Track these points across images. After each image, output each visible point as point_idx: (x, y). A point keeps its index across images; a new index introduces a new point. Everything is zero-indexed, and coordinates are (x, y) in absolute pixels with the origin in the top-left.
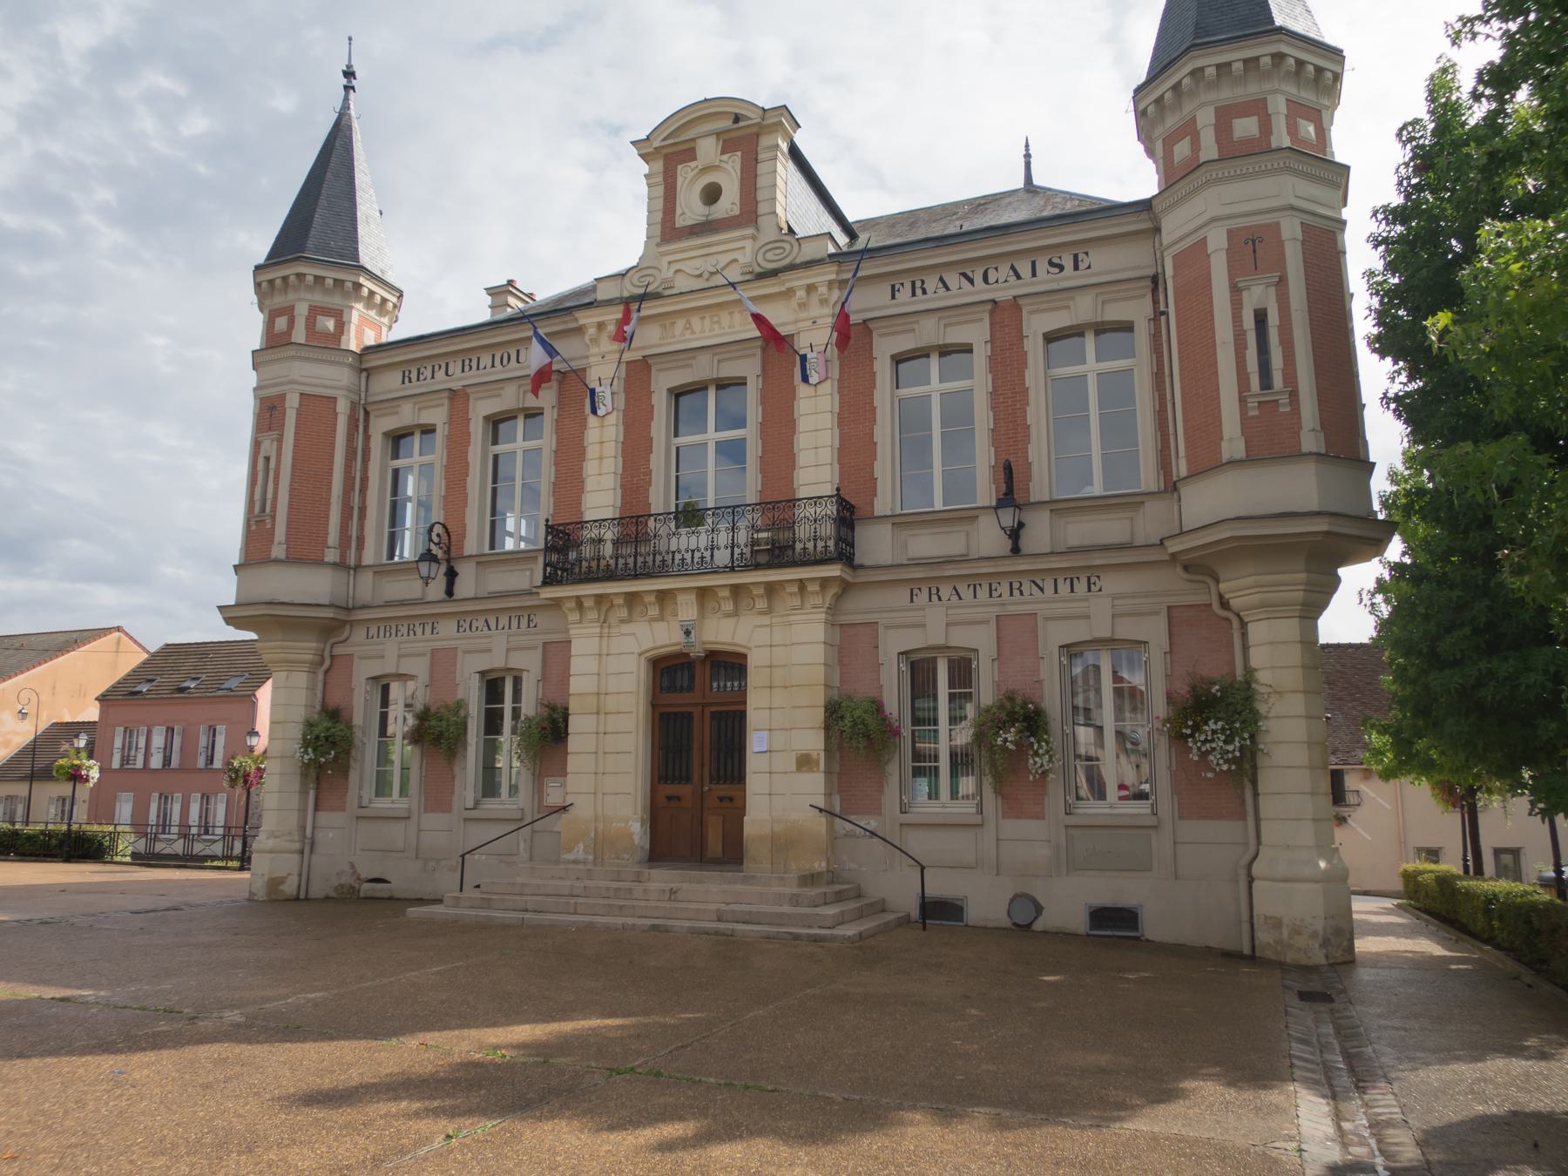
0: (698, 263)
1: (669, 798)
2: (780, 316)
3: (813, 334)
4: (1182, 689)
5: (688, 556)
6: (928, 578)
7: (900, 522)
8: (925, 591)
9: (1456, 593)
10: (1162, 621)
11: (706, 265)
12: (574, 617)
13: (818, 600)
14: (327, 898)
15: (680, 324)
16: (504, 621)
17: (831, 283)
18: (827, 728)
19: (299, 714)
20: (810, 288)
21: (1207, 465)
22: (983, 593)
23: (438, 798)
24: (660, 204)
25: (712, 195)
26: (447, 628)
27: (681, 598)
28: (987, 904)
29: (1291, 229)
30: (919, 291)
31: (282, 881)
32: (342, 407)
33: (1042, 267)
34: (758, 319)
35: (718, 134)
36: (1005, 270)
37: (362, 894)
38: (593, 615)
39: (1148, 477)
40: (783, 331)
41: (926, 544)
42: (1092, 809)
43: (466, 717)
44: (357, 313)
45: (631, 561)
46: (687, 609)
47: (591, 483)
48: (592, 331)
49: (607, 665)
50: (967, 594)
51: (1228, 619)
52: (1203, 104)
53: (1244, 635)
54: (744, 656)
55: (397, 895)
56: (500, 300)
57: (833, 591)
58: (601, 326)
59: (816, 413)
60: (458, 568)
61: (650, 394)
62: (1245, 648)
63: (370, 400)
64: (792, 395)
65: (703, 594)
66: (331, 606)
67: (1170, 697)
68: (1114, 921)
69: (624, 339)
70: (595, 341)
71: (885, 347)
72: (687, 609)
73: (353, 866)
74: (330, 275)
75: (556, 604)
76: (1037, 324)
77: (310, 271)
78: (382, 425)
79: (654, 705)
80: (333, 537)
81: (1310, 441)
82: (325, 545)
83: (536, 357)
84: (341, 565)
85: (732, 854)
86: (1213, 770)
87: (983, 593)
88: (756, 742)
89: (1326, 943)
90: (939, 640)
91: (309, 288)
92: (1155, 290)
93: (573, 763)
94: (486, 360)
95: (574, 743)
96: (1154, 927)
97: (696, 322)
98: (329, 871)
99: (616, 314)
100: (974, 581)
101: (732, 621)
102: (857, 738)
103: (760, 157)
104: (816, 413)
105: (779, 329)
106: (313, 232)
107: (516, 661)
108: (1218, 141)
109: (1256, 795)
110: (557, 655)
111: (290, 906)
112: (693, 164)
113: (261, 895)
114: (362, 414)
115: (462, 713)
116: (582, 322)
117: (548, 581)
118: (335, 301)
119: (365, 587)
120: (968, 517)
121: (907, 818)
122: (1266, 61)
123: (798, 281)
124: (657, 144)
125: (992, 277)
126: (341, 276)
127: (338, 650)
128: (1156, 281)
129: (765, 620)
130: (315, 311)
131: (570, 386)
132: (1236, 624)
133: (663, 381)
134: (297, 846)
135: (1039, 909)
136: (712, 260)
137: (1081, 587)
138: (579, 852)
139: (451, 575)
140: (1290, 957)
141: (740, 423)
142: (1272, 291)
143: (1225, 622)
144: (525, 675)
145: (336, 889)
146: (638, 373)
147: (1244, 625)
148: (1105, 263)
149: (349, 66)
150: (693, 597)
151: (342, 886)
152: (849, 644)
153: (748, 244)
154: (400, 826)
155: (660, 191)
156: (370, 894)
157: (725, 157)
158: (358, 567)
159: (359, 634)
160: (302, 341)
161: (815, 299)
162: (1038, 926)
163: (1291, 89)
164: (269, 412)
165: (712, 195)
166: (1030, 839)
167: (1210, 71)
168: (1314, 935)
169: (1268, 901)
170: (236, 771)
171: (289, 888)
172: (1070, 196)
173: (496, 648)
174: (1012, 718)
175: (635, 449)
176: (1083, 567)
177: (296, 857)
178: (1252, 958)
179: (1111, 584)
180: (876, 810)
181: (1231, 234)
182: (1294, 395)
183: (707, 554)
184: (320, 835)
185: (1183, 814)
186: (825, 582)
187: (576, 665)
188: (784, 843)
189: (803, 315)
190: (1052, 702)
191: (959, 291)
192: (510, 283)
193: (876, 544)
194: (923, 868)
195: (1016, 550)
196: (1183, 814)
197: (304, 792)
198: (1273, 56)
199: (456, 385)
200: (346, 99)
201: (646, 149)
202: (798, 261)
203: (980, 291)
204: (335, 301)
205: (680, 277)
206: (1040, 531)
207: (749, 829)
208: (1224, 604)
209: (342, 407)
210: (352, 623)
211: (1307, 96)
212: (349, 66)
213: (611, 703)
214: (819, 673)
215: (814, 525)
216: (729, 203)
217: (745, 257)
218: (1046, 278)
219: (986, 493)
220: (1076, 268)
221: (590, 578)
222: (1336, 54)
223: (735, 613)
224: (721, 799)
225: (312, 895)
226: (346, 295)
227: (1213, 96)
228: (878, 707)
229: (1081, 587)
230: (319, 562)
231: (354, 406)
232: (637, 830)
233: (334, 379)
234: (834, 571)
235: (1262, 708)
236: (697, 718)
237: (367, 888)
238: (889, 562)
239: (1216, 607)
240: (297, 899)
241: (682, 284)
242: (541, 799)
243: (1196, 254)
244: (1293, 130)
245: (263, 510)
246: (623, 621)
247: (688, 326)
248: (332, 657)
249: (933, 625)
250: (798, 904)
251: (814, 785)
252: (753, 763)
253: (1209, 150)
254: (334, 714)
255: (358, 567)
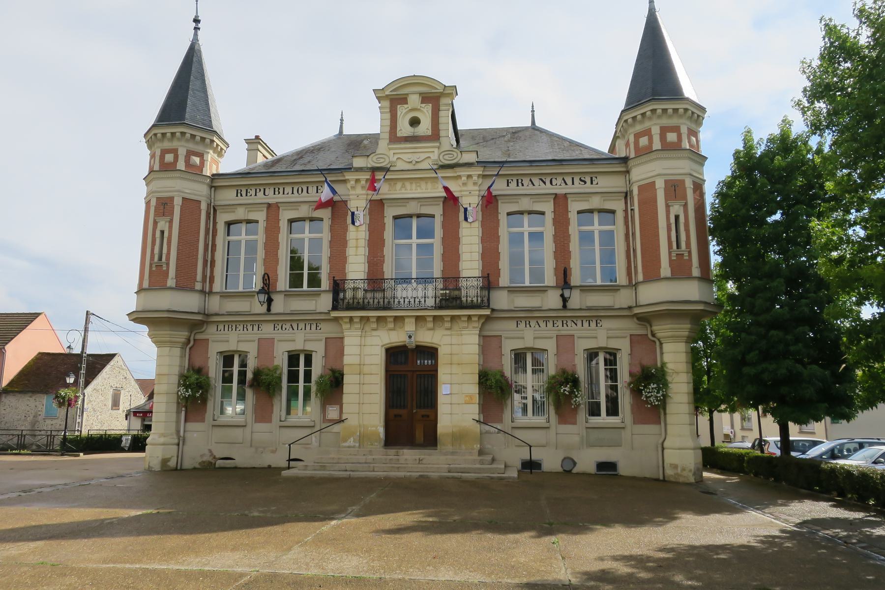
0: (409, 156)
1: (396, 416)
2: (454, 187)
3: (470, 198)
4: (637, 370)
5: (402, 301)
6: (527, 316)
7: (512, 290)
8: (524, 322)
9: (753, 337)
10: (628, 339)
11: (414, 157)
12: (346, 326)
13: (476, 325)
14: (195, 469)
15: (399, 185)
16: (302, 325)
17: (479, 176)
18: (480, 383)
19: (176, 370)
20: (469, 177)
21: (652, 275)
22: (550, 324)
23: (262, 414)
24: (388, 122)
25: (415, 122)
26: (267, 330)
27: (407, 320)
28: (551, 462)
29: (689, 184)
30: (520, 184)
31: (168, 460)
32: (204, 206)
33: (577, 181)
34: (446, 189)
35: (420, 94)
36: (559, 180)
37: (217, 466)
38: (358, 326)
39: (621, 278)
40: (456, 194)
41: (523, 301)
42: (594, 420)
43: (281, 374)
44: (210, 155)
45: (381, 301)
46: (410, 326)
47: (351, 259)
48: (353, 183)
49: (364, 354)
50: (543, 324)
51: (654, 342)
52: (655, 124)
53: (661, 348)
54: (436, 349)
55: (240, 465)
56: (253, 146)
57: (482, 321)
58: (357, 181)
59: (470, 236)
60: (273, 297)
61: (383, 217)
62: (662, 354)
63: (218, 203)
64: (457, 226)
65: (418, 318)
66: (199, 313)
67: (631, 374)
68: (607, 467)
69: (375, 190)
70: (353, 188)
71: (504, 208)
72: (410, 326)
73: (210, 451)
74: (199, 134)
75: (336, 319)
76: (574, 207)
77: (189, 131)
78: (223, 218)
79: (387, 371)
80: (199, 277)
81: (696, 272)
82: (195, 280)
83: (325, 194)
84: (202, 292)
85: (431, 440)
86: (651, 404)
87: (550, 324)
88: (443, 390)
89: (694, 474)
90: (529, 344)
91: (659, 117)
92: (626, 197)
93: (346, 398)
94: (288, 189)
95: (346, 388)
96: (624, 469)
97: (407, 184)
98: (194, 455)
99: (368, 176)
100: (546, 319)
101: (431, 332)
102: (494, 390)
103: (441, 108)
104: (470, 236)
105: (455, 194)
106: (188, 110)
107: (309, 347)
108: (661, 141)
109: (665, 414)
110: (335, 346)
111: (172, 472)
112: (406, 106)
113: (157, 468)
114: (213, 210)
115: (278, 372)
116: (347, 178)
117: (335, 308)
118: (199, 148)
119: (215, 304)
120: (543, 290)
121: (514, 425)
122: (681, 111)
123: (464, 172)
124: (387, 93)
125: (554, 182)
126: (194, 133)
127: (199, 337)
128: (627, 195)
129: (448, 332)
130: (190, 153)
131: (337, 208)
132: (658, 343)
133: (390, 212)
134: (176, 441)
135: (575, 464)
136: (417, 155)
137: (593, 324)
138: (351, 442)
139: (270, 301)
140: (681, 480)
141: (431, 235)
142: (167, 224)
143: (646, 342)
144: (314, 354)
145: (200, 464)
146: (377, 207)
147: (661, 344)
148: (606, 183)
149: (197, 16)
150: (414, 320)
151: (204, 462)
152: (489, 344)
153: (436, 150)
154: (240, 430)
155: (388, 116)
156: (222, 466)
157: (423, 105)
158: (211, 292)
159: (212, 329)
160: (184, 169)
161: (470, 182)
162: (575, 471)
163: (688, 123)
164: (160, 207)
165: (415, 122)
166: (571, 434)
167: (659, 111)
168: (690, 471)
169: (671, 457)
170: (64, 398)
171: (172, 464)
172: (573, 144)
173: (298, 339)
174: (566, 382)
175: (375, 244)
176: (595, 316)
177: (176, 447)
178: (664, 480)
179: (606, 324)
180: (501, 421)
181: (666, 182)
182: (690, 253)
183: (423, 300)
184: (188, 435)
185: (636, 421)
186: (480, 316)
187: (347, 350)
188: (459, 437)
189: (464, 188)
190: (581, 372)
191: (540, 188)
192: (257, 137)
193: (501, 300)
194: (531, 447)
195: (565, 306)
196: (636, 421)
197: (178, 412)
198: (651, 110)
199: (271, 201)
200: (196, 35)
201: (380, 95)
202: (461, 162)
203: (548, 189)
204: (199, 148)
205: (399, 161)
206: (576, 299)
207: (440, 430)
208: (653, 335)
209: (204, 206)
210: (208, 323)
211: (693, 126)
212: (197, 16)
213: (366, 369)
214: (476, 358)
215: (470, 289)
216: (425, 128)
217: (434, 156)
218: (578, 187)
219: (550, 279)
220: (592, 183)
221: (349, 308)
222: (703, 110)
223: (433, 329)
224: (423, 416)
225: (184, 467)
226: (206, 146)
227: (659, 121)
228: (503, 375)
229: (593, 324)
230: (192, 290)
231: (209, 205)
232: (381, 430)
233: (198, 190)
234: (487, 312)
235: (669, 379)
236: (411, 379)
237: (220, 463)
238: (506, 308)
239: (650, 336)
240: (176, 469)
241: (400, 165)
242: (324, 416)
243: (648, 189)
244: (689, 142)
245: (160, 259)
246: (374, 330)
247: (403, 186)
248: (195, 340)
249: (527, 337)
250: (483, 464)
251: (474, 410)
252: (441, 399)
253: (657, 145)
254: (199, 371)
255: (211, 292)
